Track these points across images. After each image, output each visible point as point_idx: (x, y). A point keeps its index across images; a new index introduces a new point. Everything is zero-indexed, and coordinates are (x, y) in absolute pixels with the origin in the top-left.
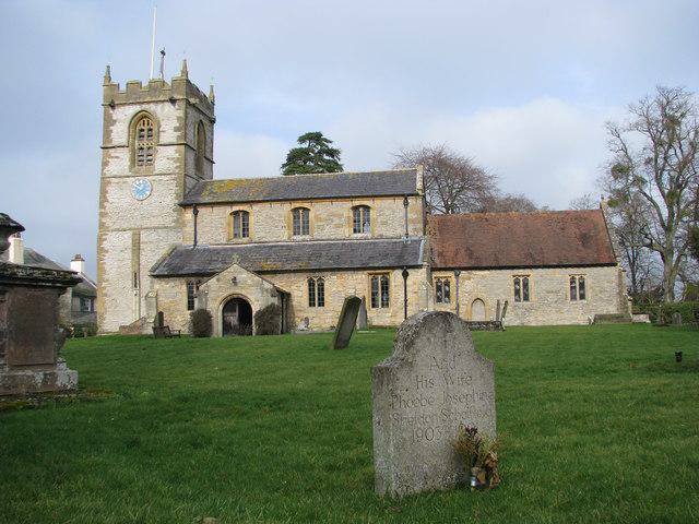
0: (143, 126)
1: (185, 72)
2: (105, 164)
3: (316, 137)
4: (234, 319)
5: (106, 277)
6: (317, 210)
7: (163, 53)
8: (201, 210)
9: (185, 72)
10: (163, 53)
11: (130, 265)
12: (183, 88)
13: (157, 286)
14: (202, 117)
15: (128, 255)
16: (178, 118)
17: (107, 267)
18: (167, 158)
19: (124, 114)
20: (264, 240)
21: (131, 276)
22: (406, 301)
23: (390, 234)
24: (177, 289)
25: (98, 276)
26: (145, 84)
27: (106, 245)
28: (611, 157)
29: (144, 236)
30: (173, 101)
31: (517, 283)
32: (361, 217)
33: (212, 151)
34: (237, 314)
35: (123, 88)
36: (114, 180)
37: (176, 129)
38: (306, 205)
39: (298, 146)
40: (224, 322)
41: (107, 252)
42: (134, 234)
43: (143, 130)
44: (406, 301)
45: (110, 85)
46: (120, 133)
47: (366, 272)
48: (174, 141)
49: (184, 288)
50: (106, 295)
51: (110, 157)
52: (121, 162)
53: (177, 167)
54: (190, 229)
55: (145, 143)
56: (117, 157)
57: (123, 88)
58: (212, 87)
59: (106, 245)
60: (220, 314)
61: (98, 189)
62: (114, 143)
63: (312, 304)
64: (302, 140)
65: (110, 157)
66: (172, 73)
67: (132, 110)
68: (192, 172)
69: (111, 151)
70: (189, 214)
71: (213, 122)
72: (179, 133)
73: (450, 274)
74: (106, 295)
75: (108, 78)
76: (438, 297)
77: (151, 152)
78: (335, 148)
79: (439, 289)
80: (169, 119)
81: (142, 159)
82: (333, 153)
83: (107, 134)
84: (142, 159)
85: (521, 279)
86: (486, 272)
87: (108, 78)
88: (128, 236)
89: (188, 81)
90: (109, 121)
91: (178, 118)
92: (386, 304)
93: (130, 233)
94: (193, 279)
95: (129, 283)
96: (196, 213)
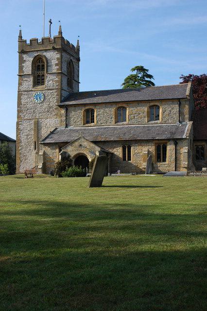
0: (40, 66)
1: (60, 33)
2: (20, 84)
3: (141, 69)
7: (50, 22)
8: (70, 109)
9: (60, 33)
10: (50, 22)
12: (60, 41)
14: (72, 58)
16: (58, 59)
18: (52, 81)
19: (29, 59)
25: (17, 136)
26: (40, 41)
27: (21, 127)
30: (54, 49)
33: (78, 77)
35: (28, 42)
37: (56, 65)
38: (124, 105)
43: (39, 66)
45: (21, 41)
46: (28, 68)
47: (154, 142)
51: (22, 80)
52: (29, 83)
53: (57, 86)
55: (40, 73)
57: (28, 42)
58: (20, 31)
59: (21, 127)
64: (133, 70)
66: (55, 33)
68: (65, 87)
70: (63, 111)
71: (78, 60)
72: (58, 67)
73: (203, 143)
75: (20, 37)
76: (197, 156)
77: (43, 78)
79: (198, 152)
80: (53, 57)
81: (39, 80)
82: (150, 76)
83: (21, 68)
84: (39, 80)
87: (20, 37)
89: (62, 38)
90: (21, 61)
92: (164, 160)
93: (33, 122)
96: (67, 110)
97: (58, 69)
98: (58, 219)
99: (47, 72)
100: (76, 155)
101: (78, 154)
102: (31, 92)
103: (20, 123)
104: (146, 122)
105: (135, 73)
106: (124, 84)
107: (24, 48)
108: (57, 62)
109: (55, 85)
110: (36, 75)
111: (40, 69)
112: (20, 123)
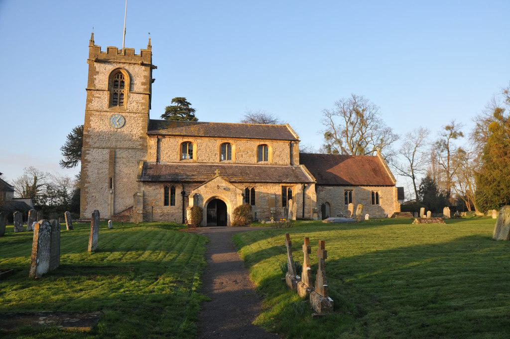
0: (116, 80)
2: (89, 101)
3: (181, 101)
4: (214, 213)
5: (88, 180)
6: (271, 147)
7: (149, 33)
11: (107, 172)
13: (143, 189)
15: (106, 165)
16: (145, 77)
17: (89, 173)
20: (205, 161)
21: (107, 181)
22: (304, 203)
23: (281, 163)
24: (157, 191)
28: (326, 128)
29: (119, 154)
31: (346, 194)
32: (225, 149)
34: (216, 210)
36: (95, 113)
37: (143, 84)
39: (170, 104)
40: (208, 215)
41: (90, 162)
42: (111, 152)
44: (304, 203)
45: (94, 48)
46: (103, 81)
48: (141, 91)
49: (162, 190)
50: (88, 193)
53: (143, 109)
54: (153, 151)
56: (98, 97)
58: (93, 34)
60: (206, 209)
61: (205, 121)
62: (134, 91)
63: (166, 204)
64: (173, 100)
65: (93, 96)
67: (110, 68)
69: (93, 92)
72: (145, 87)
74: (88, 193)
75: (92, 41)
78: (193, 108)
83: (91, 81)
85: (349, 192)
86: (331, 188)
87: (92, 41)
88: (106, 154)
90: (92, 72)
91: (145, 77)
94: (169, 185)
95: (106, 185)
96: (159, 141)
97: (145, 89)
98: (449, 277)
99: (130, 90)
100: (210, 199)
101: (214, 197)
102: (105, 113)
103: (87, 152)
104: (256, 161)
105: (175, 104)
106: (242, 122)
107: (98, 58)
108: (144, 81)
109: (140, 108)
110: (113, 92)
111: (117, 85)
112: (87, 152)
